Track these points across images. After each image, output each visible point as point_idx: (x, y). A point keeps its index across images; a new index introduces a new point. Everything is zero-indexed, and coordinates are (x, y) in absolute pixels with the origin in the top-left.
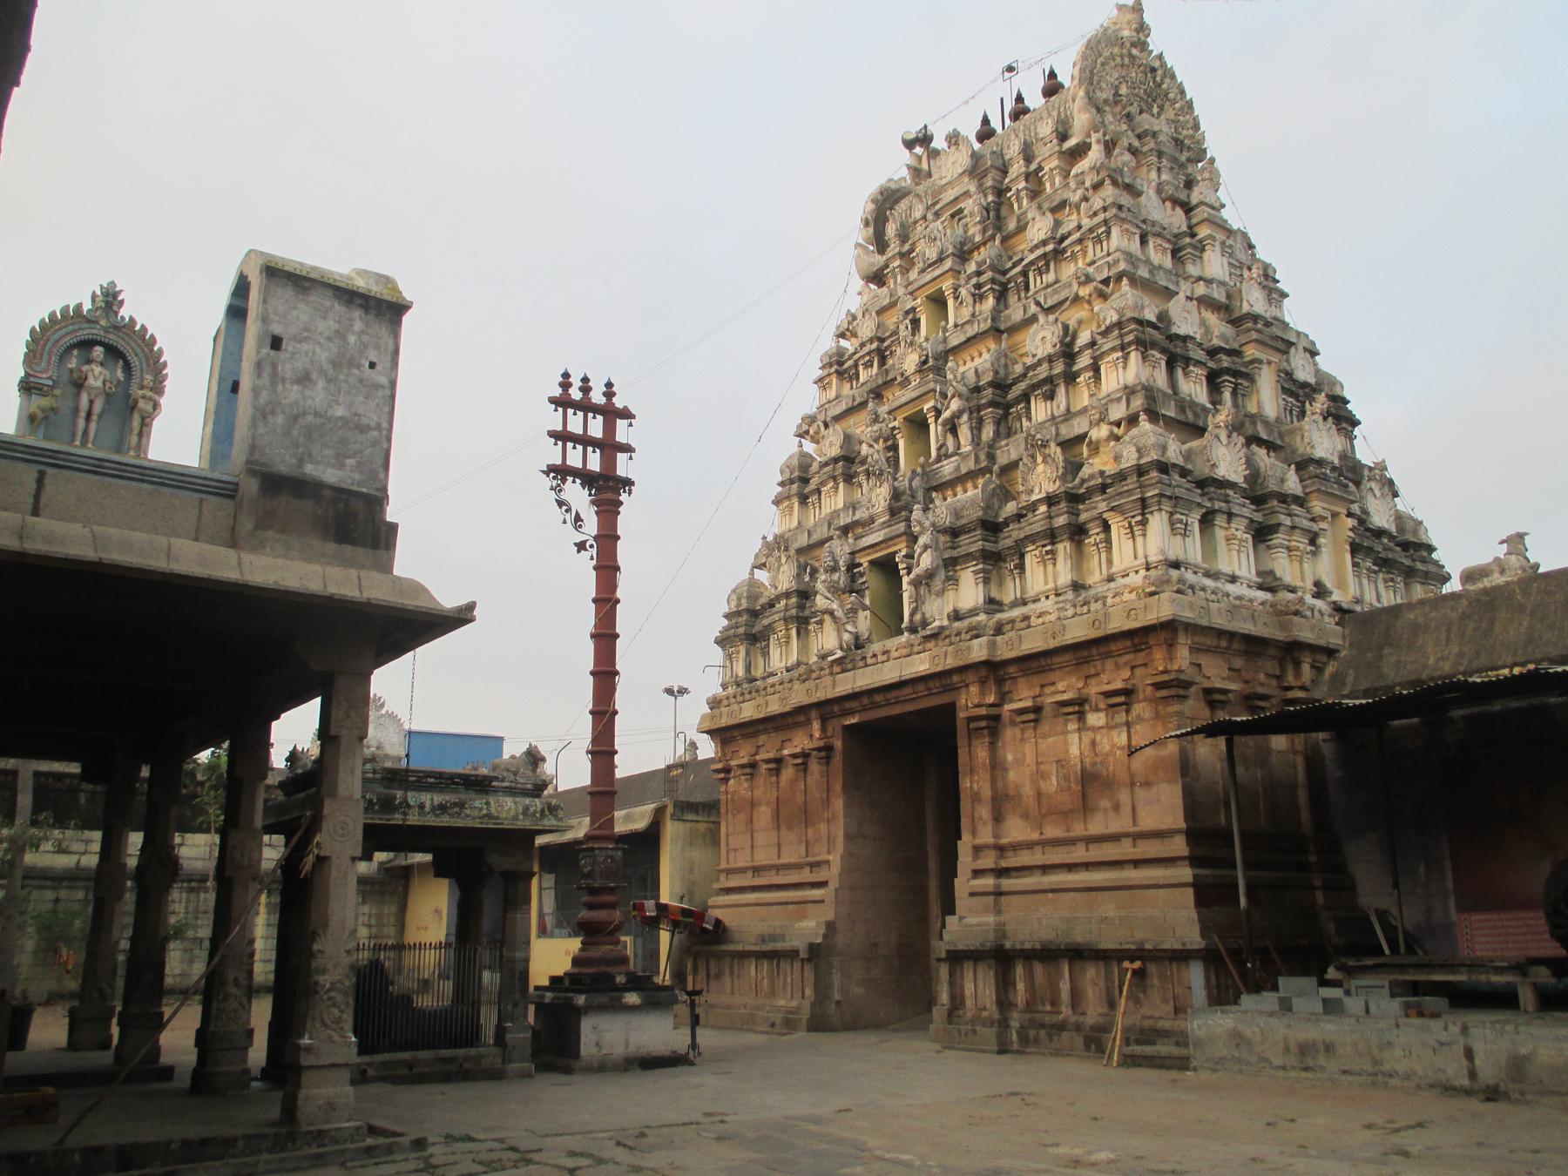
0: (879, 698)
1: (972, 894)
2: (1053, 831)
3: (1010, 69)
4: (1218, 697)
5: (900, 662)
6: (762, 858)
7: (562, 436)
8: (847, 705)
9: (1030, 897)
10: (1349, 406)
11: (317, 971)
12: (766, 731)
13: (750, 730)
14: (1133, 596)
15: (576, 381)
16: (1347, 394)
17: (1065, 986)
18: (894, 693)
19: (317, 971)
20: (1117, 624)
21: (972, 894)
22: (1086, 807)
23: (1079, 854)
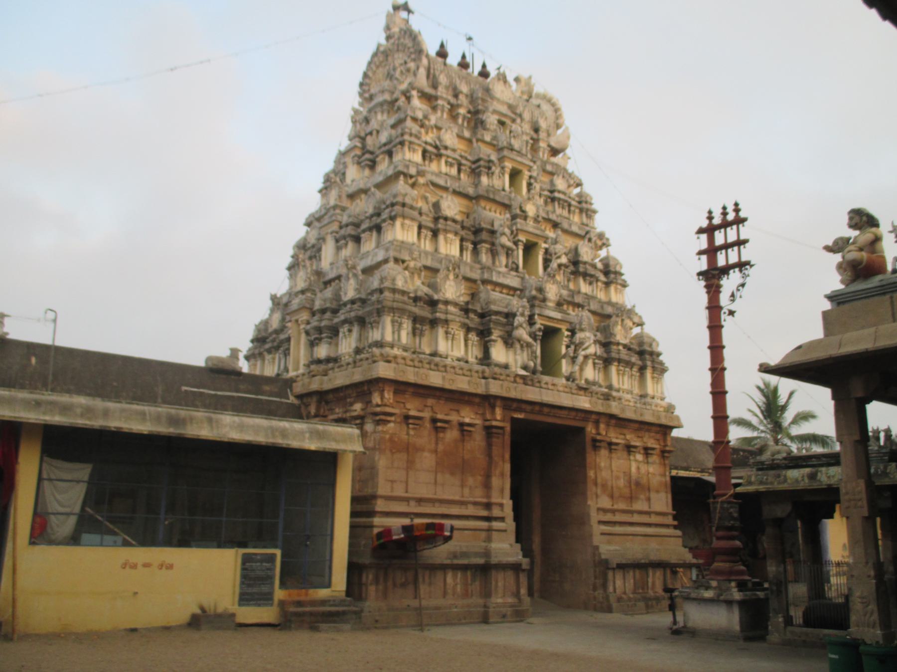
0: (546, 410)
1: (602, 534)
2: (622, 506)
3: (470, 39)
4: (466, 428)
5: (554, 393)
6: (424, 492)
7: (740, 243)
8: (524, 406)
9: (621, 537)
10: (661, 358)
11: (215, 610)
12: (434, 397)
13: (422, 391)
14: (662, 409)
15: (730, 209)
16: (660, 349)
17: (650, 580)
18: (556, 411)
19: (215, 610)
20: (648, 418)
21: (602, 534)
22: (631, 498)
23: (636, 518)
